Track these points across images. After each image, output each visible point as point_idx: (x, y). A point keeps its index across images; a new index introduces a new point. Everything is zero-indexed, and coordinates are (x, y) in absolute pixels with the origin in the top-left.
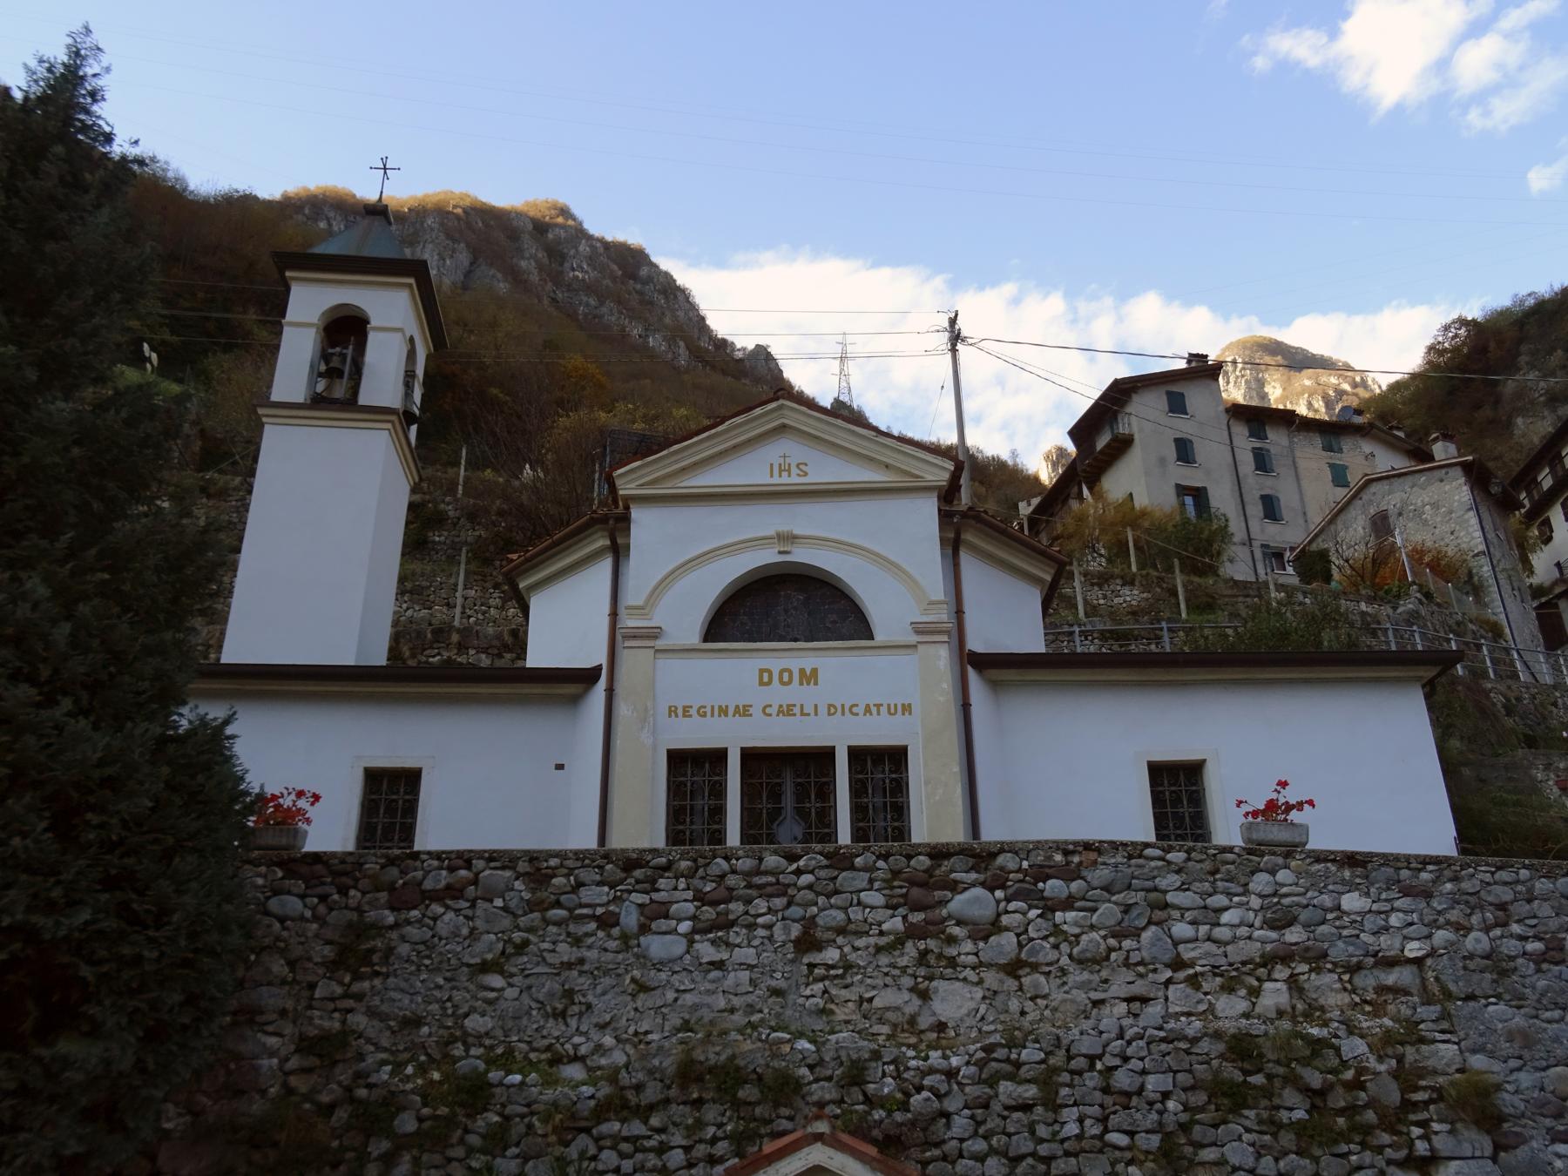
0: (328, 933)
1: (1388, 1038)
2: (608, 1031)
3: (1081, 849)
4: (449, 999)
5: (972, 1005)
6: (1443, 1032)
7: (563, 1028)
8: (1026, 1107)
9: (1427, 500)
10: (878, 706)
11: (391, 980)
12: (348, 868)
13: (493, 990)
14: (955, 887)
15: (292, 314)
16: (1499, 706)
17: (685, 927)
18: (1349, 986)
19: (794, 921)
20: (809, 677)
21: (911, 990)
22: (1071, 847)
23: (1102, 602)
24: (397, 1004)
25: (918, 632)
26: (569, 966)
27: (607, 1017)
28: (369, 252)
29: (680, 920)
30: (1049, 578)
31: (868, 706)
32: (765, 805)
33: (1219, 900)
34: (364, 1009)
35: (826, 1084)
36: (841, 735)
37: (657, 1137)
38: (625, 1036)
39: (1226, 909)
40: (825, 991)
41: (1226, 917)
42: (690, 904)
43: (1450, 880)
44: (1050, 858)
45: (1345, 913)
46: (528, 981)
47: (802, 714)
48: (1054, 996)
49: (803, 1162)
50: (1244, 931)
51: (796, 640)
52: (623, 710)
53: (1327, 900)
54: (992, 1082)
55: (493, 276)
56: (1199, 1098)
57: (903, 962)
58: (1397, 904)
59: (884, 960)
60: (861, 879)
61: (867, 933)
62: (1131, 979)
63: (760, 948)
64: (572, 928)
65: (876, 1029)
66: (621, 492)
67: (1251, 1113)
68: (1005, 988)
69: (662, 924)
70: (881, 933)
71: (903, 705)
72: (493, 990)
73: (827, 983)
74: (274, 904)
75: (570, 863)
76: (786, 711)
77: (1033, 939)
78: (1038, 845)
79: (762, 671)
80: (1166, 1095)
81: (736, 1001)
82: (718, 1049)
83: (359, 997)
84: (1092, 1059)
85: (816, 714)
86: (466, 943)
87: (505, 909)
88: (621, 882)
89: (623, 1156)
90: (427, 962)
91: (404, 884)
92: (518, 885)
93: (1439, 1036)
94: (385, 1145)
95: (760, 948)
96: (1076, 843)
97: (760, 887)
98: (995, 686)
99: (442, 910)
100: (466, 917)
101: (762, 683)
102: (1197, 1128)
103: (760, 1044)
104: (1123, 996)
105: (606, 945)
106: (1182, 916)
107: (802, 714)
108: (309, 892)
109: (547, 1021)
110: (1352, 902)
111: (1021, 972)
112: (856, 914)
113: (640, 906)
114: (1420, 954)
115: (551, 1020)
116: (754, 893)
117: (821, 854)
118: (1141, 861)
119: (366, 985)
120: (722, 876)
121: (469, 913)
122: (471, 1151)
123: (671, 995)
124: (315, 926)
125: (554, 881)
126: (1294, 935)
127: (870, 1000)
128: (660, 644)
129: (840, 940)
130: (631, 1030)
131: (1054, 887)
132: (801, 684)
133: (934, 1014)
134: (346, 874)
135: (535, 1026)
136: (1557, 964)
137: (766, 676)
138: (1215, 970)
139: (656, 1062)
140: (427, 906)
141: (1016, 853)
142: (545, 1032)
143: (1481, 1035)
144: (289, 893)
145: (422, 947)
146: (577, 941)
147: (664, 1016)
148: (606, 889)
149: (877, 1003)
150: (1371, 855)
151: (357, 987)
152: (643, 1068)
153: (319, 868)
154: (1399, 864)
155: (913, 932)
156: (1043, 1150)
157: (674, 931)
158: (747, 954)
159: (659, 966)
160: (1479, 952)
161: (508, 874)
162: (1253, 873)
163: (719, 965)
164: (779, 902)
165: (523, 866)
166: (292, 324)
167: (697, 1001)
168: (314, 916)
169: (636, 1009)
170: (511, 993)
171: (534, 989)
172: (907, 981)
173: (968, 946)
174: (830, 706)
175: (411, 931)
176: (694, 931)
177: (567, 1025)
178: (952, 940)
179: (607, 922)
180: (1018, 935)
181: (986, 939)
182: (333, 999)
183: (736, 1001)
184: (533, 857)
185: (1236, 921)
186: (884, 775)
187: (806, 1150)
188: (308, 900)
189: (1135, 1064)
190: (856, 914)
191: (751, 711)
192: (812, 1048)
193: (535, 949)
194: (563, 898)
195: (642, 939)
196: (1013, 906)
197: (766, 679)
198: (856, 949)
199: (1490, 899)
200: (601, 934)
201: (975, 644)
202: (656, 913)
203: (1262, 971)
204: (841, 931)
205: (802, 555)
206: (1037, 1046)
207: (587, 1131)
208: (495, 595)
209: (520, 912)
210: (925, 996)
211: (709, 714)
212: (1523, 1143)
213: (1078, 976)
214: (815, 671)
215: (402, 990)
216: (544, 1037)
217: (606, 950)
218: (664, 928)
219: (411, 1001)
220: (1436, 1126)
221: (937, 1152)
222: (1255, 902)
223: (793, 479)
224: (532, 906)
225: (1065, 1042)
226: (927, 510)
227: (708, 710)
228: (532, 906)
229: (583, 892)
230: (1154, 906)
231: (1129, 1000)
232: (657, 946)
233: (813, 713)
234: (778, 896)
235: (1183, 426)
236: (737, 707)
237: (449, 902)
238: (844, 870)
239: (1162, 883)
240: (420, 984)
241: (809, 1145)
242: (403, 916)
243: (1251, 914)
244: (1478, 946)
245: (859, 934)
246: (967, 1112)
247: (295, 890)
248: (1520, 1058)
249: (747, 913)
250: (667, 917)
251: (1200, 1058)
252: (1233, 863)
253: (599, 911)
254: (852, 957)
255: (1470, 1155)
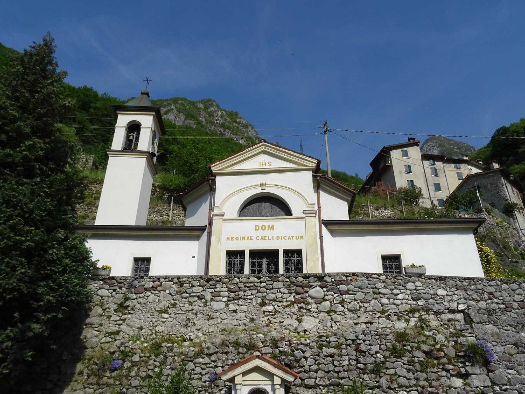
0: (115, 301)
1: (452, 335)
2: (200, 331)
3: (351, 275)
4: (151, 321)
5: (315, 324)
6: (470, 333)
7: (186, 330)
8: (332, 356)
9: (489, 182)
10: (293, 237)
11: (134, 315)
12: (122, 281)
13: (165, 318)
14: (311, 287)
15: (118, 124)
16: (512, 248)
17: (225, 299)
18: (439, 319)
19: (259, 297)
20: (271, 228)
21: (296, 319)
22: (348, 275)
23: (378, 215)
24: (135, 322)
25: (304, 213)
26: (189, 311)
27: (200, 327)
28: (142, 105)
29: (223, 297)
30: (350, 199)
31: (289, 236)
32: (257, 268)
33: (396, 291)
34: (125, 324)
35: (267, 348)
36: (281, 246)
37: (213, 363)
38: (205, 333)
39: (399, 294)
40: (268, 320)
41: (400, 297)
42: (226, 292)
43: (473, 285)
44: (341, 278)
45: (438, 295)
46: (176, 316)
47: (269, 239)
48: (342, 322)
49: (252, 365)
50: (404, 301)
51: (267, 216)
52: (213, 238)
53: (432, 291)
54: (320, 347)
55: (192, 123)
56: (387, 354)
57: (294, 310)
58: (456, 293)
59: (287, 310)
60: (281, 285)
61: (282, 301)
62: (367, 316)
63: (248, 306)
64: (190, 299)
65: (284, 331)
66: (213, 172)
67: (406, 359)
68: (326, 319)
69: (218, 298)
70: (287, 301)
71: (301, 236)
72: (165, 318)
73: (269, 317)
74: (100, 292)
75: (190, 280)
76: (264, 238)
77: (336, 304)
78: (337, 274)
79: (256, 226)
80: (377, 352)
81: (240, 322)
82: (233, 336)
83: (124, 320)
84: (353, 341)
85: (273, 239)
86: (157, 304)
87: (170, 294)
88: (205, 285)
89: (203, 369)
90: (145, 310)
91: (139, 286)
92: (174, 286)
93: (468, 335)
94: (129, 364)
95: (248, 306)
96: (349, 273)
97: (248, 287)
98: (333, 233)
99: (150, 294)
100: (157, 296)
101: (256, 230)
102: (387, 363)
103: (246, 335)
104: (364, 322)
105: (200, 305)
106: (384, 296)
107: (269, 239)
108: (110, 288)
109: (181, 328)
110: (441, 292)
111: (331, 314)
112: (279, 295)
113: (211, 293)
114: (463, 308)
115: (182, 328)
116: (247, 289)
117: (268, 277)
118: (371, 279)
119: (126, 316)
120: (237, 284)
121: (158, 295)
122: (155, 366)
123: (219, 320)
124: (112, 299)
125: (185, 285)
126: (420, 303)
127: (283, 322)
128: (224, 218)
129: (274, 303)
130: (207, 331)
131: (343, 287)
132: (268, 230)
133: (303, 327)
134: (121, 283)
135: (177, 330)
136: (509, 312)
137: (257, 227)
138: (396, 314)
139: (214, 340)
140: (146, 293)
141: (330, 277)
142: (180, 332)
143: (483, 334)
144: (104, 288)
145: (143, 305)
146: (191, 304)
147: (217, 326)
148: (201, 287)
149: (285, 323)
150: (447, 277)
151: (124, 317)
152: (210, 342)
153: (114, 281)
154: (456, 280)
155: (296, 302)
156: (337, 369)
157: (221, 301)
158: (244, 308)
159: (216, 311)
160: (483, 308)
161: (171, 283)
162: (407, 283)
163: (235, 311)
164: (254, 292)
165: (176, 280)
166: (123, 127)
167: (228, 322)
168: (111, 296)
169: (209, 325)
170: (170, 319)
171: (177, 318)
172: (295, 317)
173: (314, 306)
174: (277, 237)
175: (140, 300)
176: (228, 301)
177: (187, 329)
178: (308, 304)
179: (200, 298)
180: (331, 302)
181: (320, 303)
182: (116, 321)
183: (240, 322)
184: (179, 278)
185: (402, 298)
186: (295, 258)
187: (254, 361)
188: (110, 291)
189: (367, 342)
190: (279, 295)
191: (253, 238)
192: (263, 336)
193: (179, 306)
194: (187, 290)
195: (211, 303)
196: (330, 293)
197: (257, 228)
198: (278, 306)
199: (487, 291)
200: (199, 301)
201: (325, 217)
202: (216, 295)
203: (410, 315)
204: (274, 300)
205: (268, 190)
206: (335, 336)
207: (192, 361)
208: (183, 212)
209: (173, 295)
210: (300, 321)
211: (239, 239)
212: (497, 369)
213: (349, 314)
214: (273, 226)
215: (137, 318)
216: (180, 333)
217: (200, 306)
218: (218, 300)
219: (140, 322)
220: (467, 364)
221: (303, 370)
222: (408, 292)
223: (267, 167)
224: (178, 293)
225: (344, 335)
226: (309, 175)
227: (239, 238)
228: (178, 293)
229: (194, 288)
230: (374, 293)
231: (366, 323)
232: (215, 305)
233: (272, 239)
234: (254, 290)
235: (408, 161)
236: (248, 237)
237: (152, 291)
238: (275, 282)
239: (377, 286)
240: (142, 316)
241: (254, 359)
242: (138, 296)
243: (407, 296)
244: (483, 306)
245: (279, 302)
246: (312, 357)
247: (106, 288)
248: (496, 342)
249: (244, 295)
250: (220, 296)
251: (389, 341)
252: (401, 279)
253: (198, 294)
254: (277, 309)
255: (479, 373)
